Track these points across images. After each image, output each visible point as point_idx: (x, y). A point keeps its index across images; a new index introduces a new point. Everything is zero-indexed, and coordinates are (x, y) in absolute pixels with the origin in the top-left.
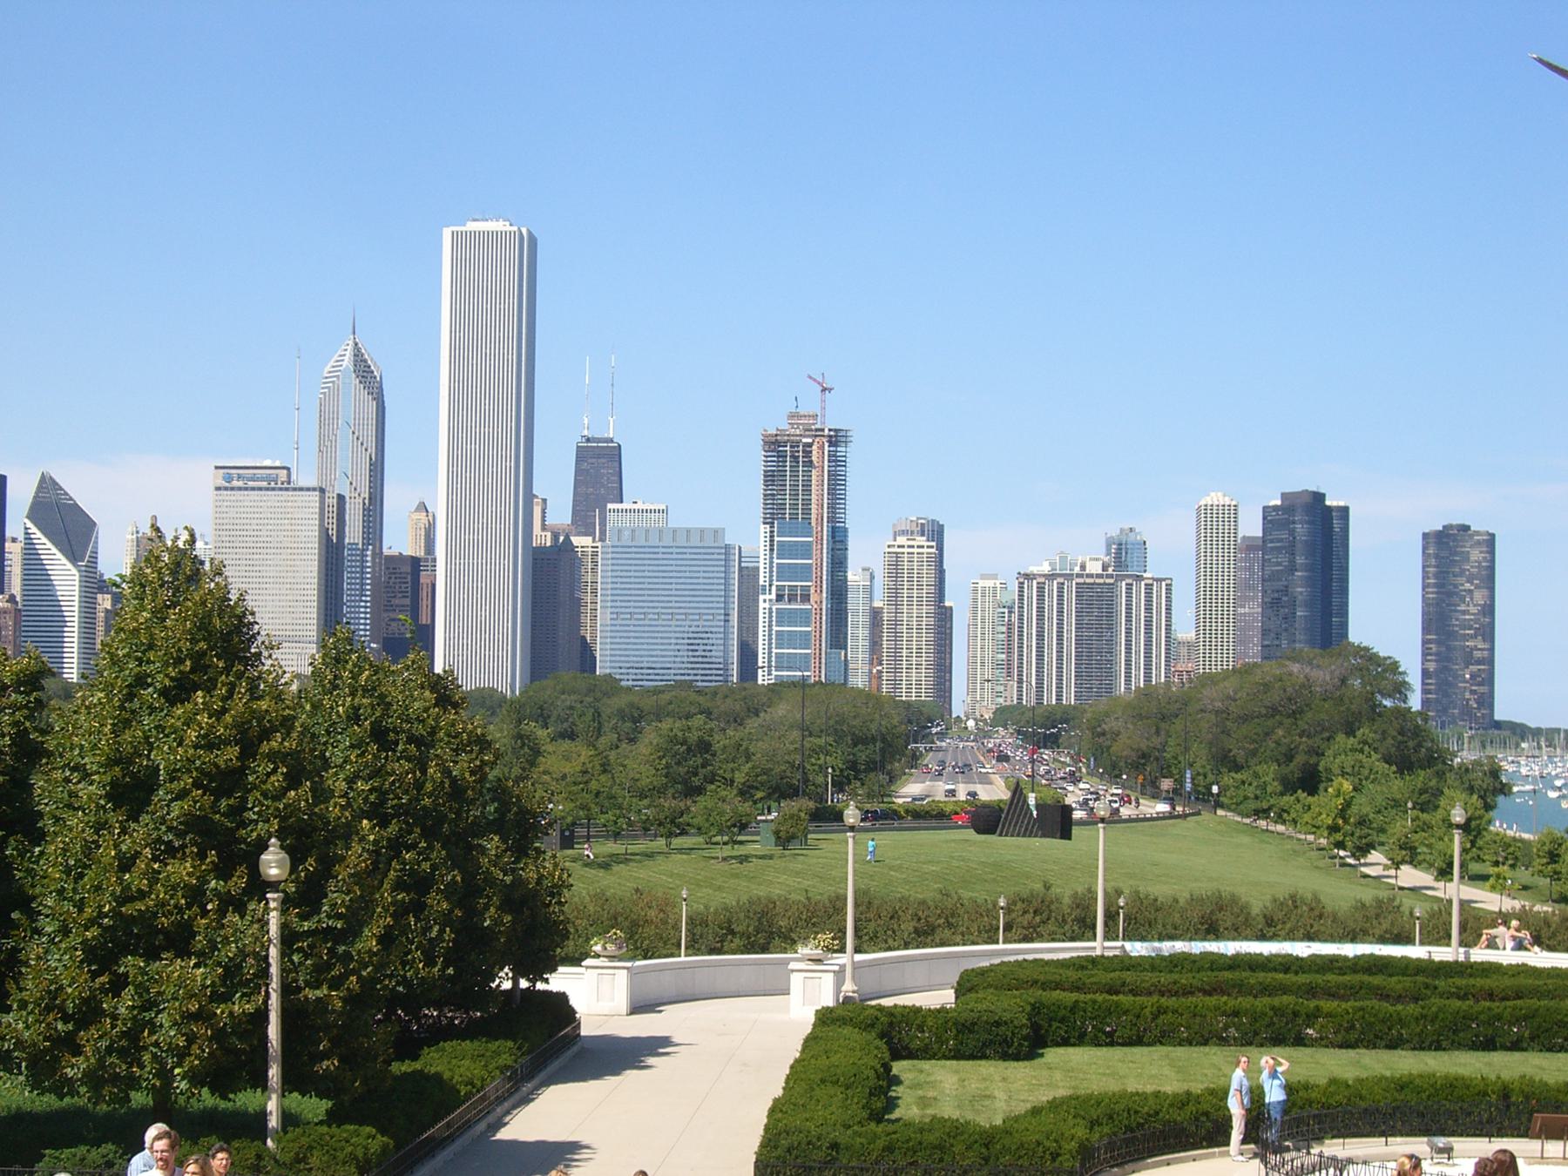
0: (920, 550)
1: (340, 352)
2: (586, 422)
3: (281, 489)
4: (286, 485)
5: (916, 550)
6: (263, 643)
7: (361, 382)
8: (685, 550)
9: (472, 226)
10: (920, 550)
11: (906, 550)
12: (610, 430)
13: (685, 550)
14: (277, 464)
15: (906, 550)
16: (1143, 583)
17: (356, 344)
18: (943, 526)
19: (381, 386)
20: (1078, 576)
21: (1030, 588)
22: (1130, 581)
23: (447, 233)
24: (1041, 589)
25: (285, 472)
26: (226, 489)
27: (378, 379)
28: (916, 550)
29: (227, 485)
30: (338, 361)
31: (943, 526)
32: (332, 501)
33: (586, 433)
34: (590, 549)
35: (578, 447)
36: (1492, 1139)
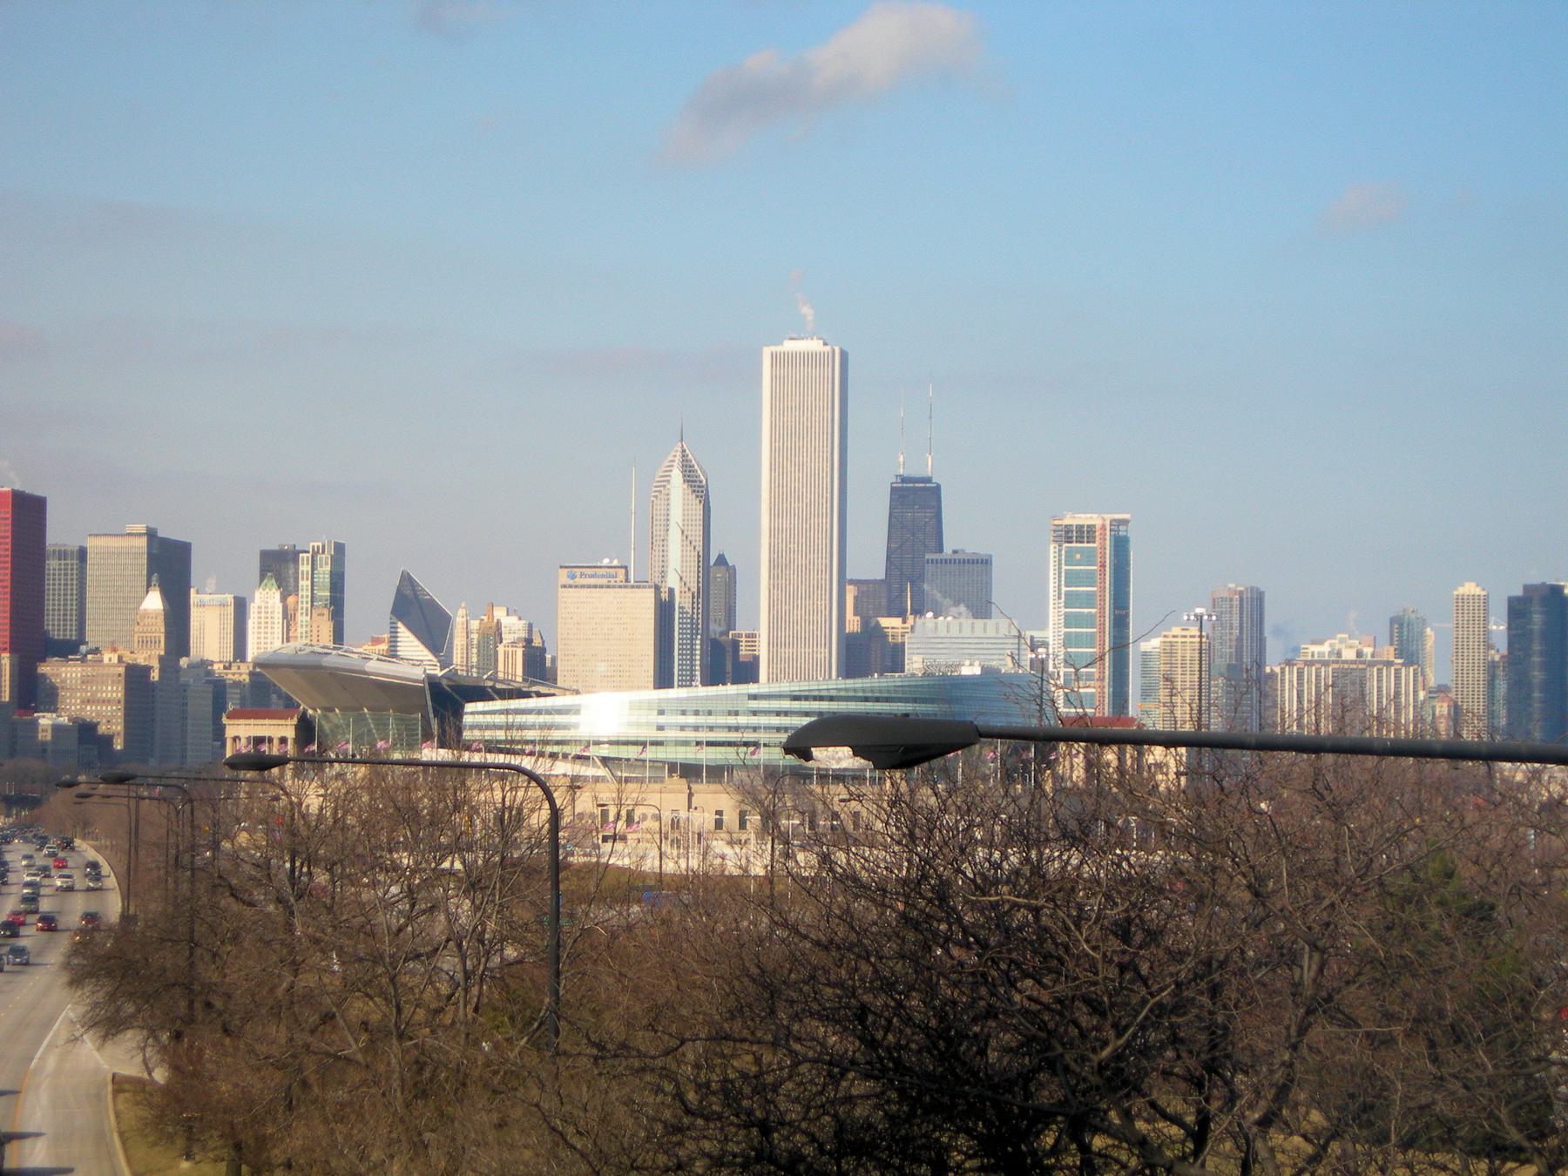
0: (1184, 640)
1: (670, 458)
2: (901, 459)
3: (620, 587)
4: (624, 583)
5: (1189, 640)
6: (1314, 920)
7: (697, 496)
8: (982, 641)
9: (789, 346)
10: (1184, 640)
11: (1180, 640)
12: (927, 467)
13: (982, 641)
14: (615, 563)
15: (1180, 640)
16: (1393, 669)
17: (684, 451)
18: (1263, 592)
19: (707, 491)
20: (1334, 662)
21: (1291, 672)
22: (1379, 666)
23: (767, 352)
24: (1300, 674)
25: (623, 571)
26: (570, 586)
27: (704, 482)
28: (1189, 640)
29: (571, 582)
30: (666, 471)
31: (1263, 592)
32: (665, 596)
33: (901, 471)
34: (900, 630)
35: (892, 488)
36: (292, 548)
